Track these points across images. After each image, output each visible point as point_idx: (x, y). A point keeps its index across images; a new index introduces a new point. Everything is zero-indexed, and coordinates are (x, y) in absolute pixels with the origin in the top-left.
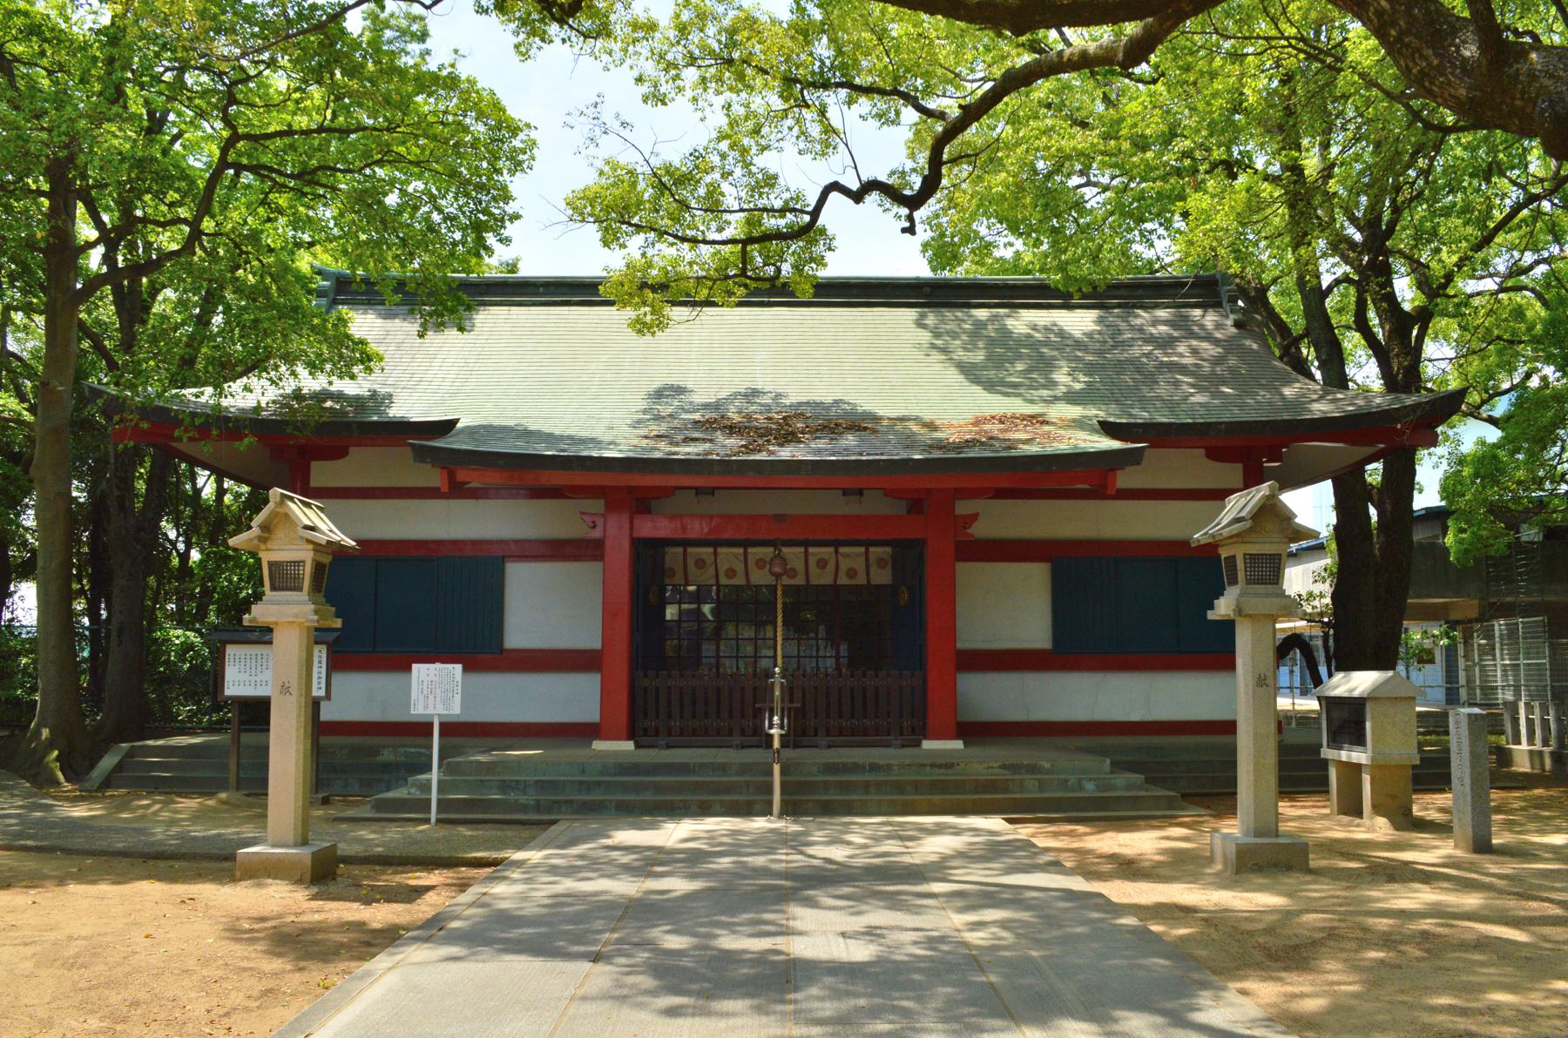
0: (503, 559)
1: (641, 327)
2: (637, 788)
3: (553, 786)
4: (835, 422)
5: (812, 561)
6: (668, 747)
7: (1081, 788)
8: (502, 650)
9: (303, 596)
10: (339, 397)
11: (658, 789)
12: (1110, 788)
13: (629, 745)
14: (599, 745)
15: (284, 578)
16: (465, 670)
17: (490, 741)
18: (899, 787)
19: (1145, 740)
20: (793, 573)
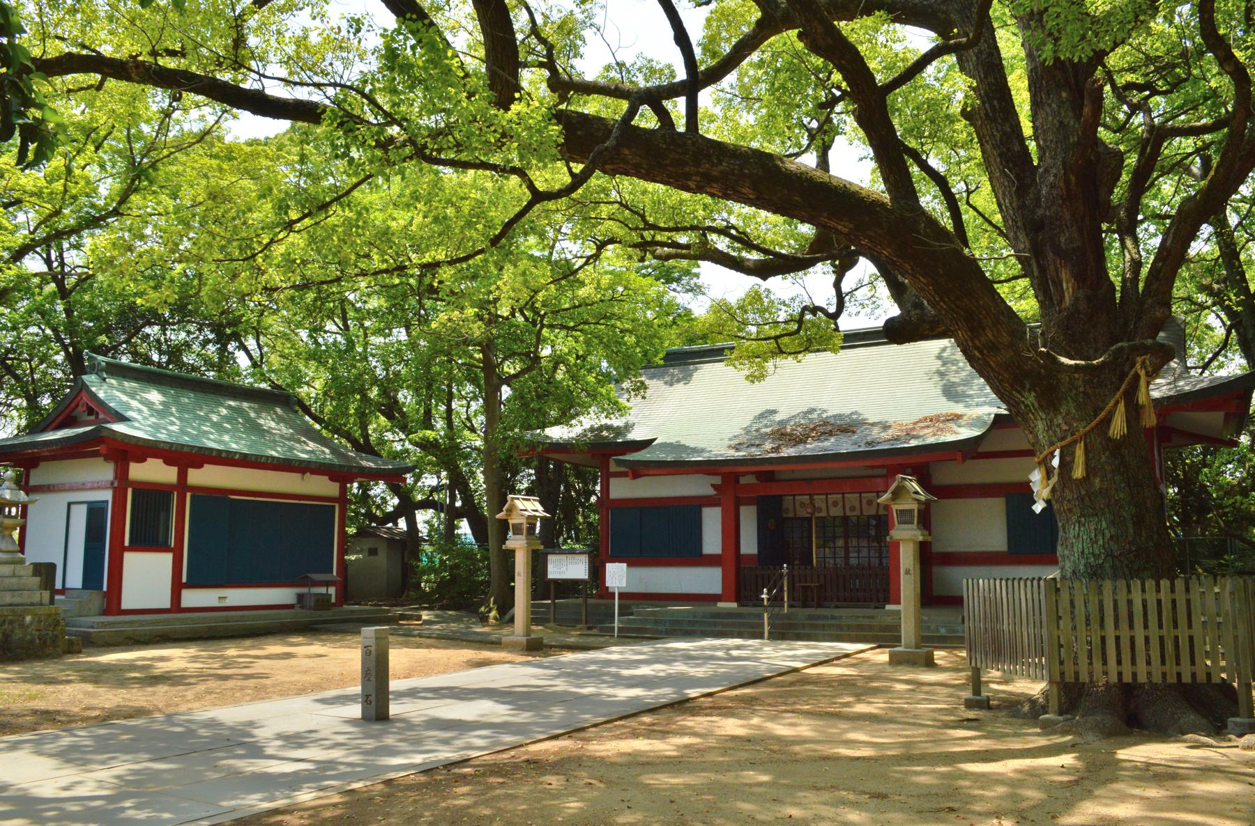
0: (701, 506)
1: (752, 378)
2: (715, 624)
3: (678, 622)
4: (846, 426)
5: (864, 501)
6: (837, 607)
7: (938, 631)
8: (701, 555)
9: (523, 537)
10: (608, 428)
11: (724, 625)
12: (954, 631)
13: (734, 605)
14: (721, 605)
15: (517, 530)
16: (629, 566)
17: (662, 603)
18: (840, 627)
19: (246, 613)
20: (820, 510)
